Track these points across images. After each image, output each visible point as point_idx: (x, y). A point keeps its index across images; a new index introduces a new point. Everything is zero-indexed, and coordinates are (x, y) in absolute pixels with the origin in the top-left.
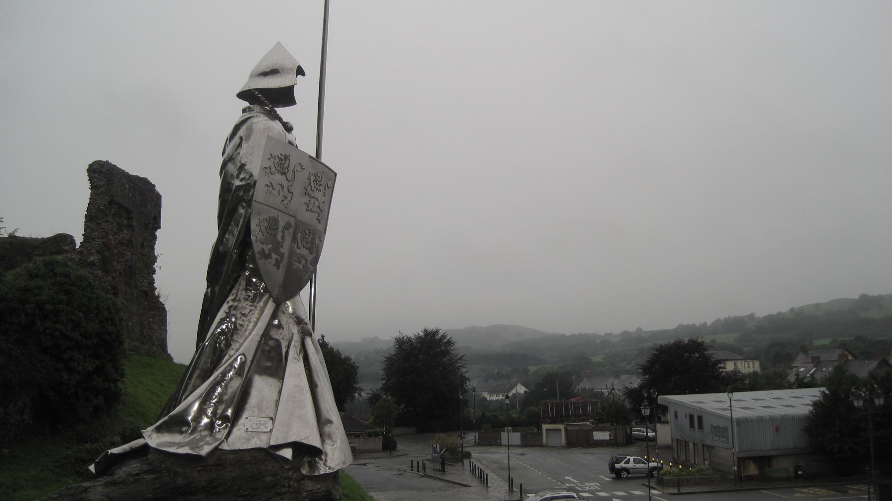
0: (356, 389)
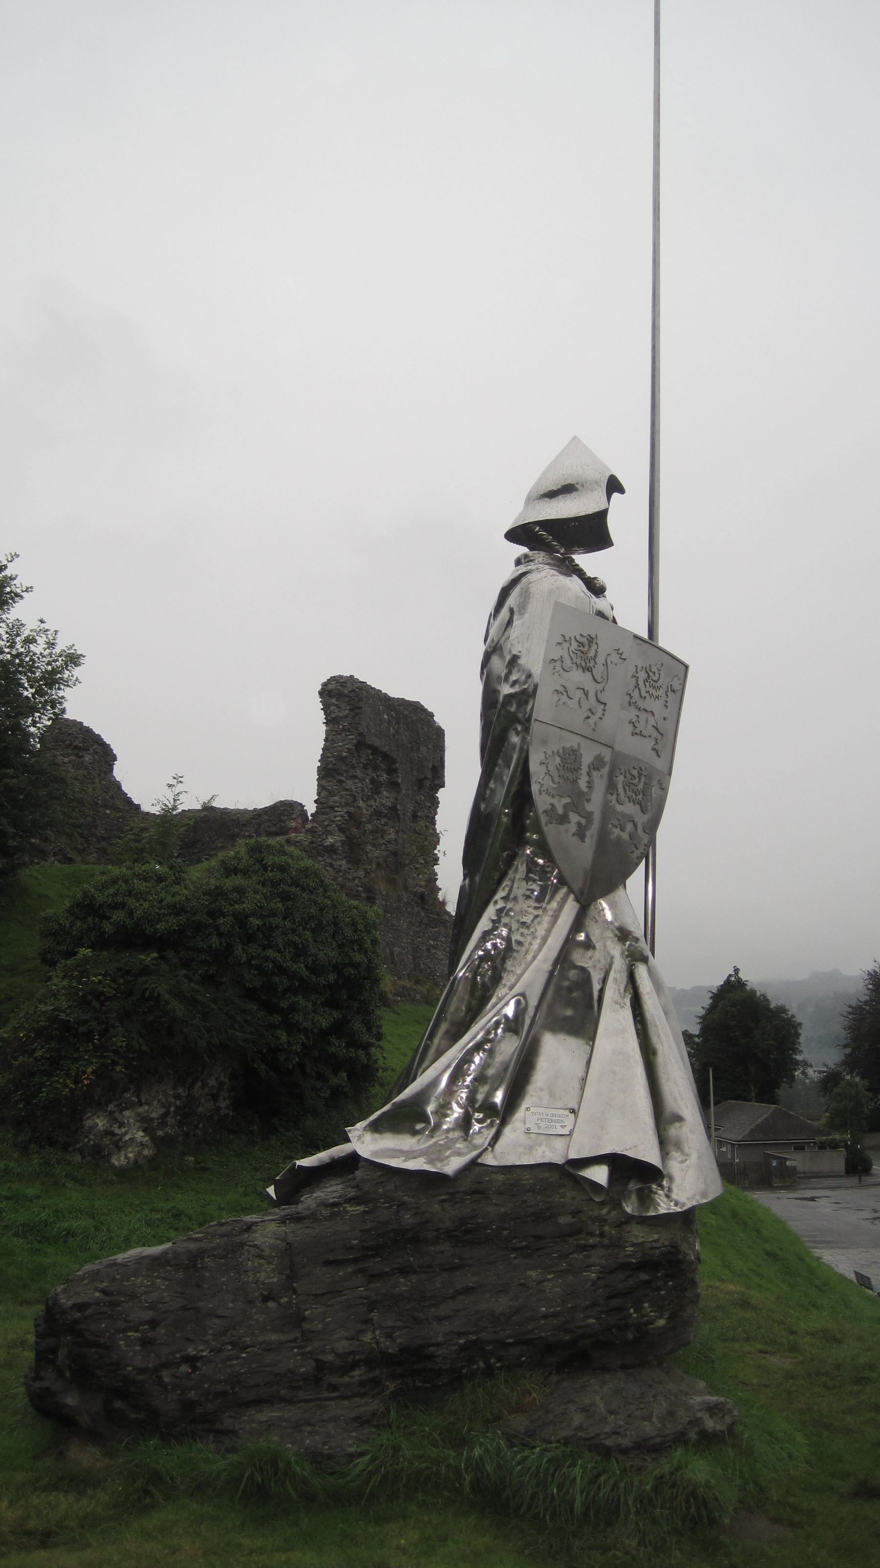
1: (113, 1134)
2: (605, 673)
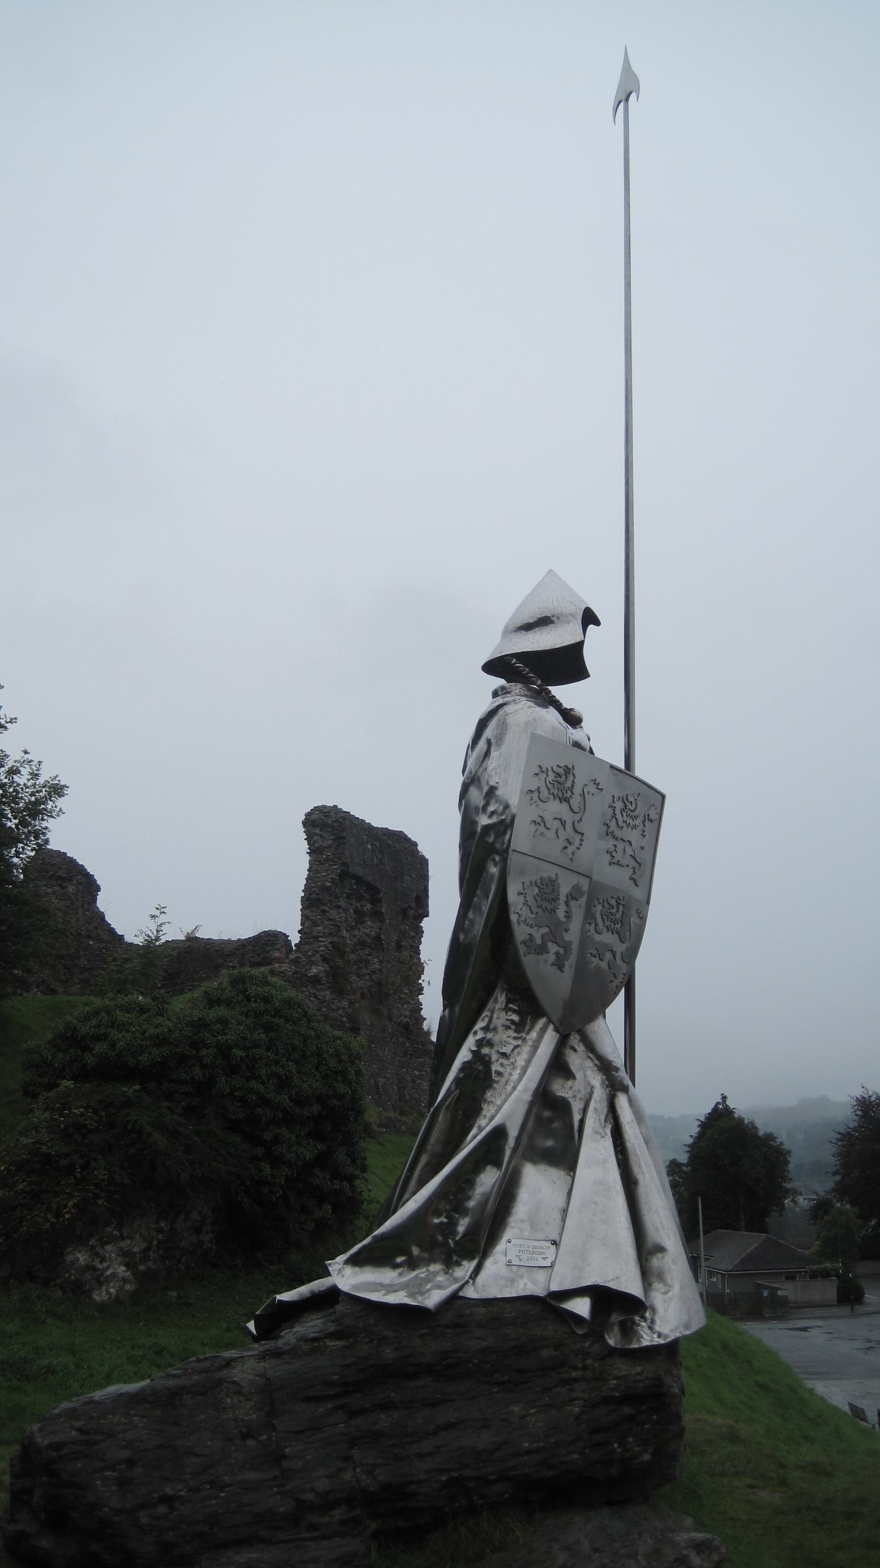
0: (786, 1192)
1: (95, 1269)
2: (582, 803)
